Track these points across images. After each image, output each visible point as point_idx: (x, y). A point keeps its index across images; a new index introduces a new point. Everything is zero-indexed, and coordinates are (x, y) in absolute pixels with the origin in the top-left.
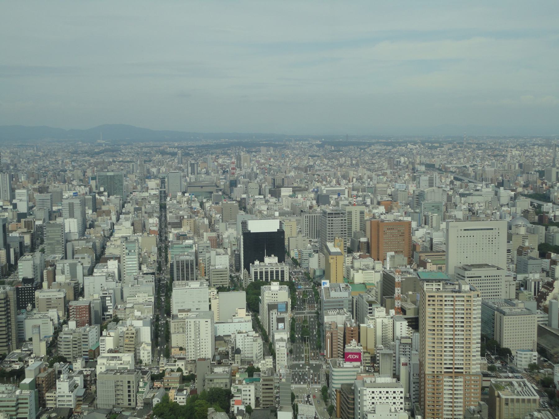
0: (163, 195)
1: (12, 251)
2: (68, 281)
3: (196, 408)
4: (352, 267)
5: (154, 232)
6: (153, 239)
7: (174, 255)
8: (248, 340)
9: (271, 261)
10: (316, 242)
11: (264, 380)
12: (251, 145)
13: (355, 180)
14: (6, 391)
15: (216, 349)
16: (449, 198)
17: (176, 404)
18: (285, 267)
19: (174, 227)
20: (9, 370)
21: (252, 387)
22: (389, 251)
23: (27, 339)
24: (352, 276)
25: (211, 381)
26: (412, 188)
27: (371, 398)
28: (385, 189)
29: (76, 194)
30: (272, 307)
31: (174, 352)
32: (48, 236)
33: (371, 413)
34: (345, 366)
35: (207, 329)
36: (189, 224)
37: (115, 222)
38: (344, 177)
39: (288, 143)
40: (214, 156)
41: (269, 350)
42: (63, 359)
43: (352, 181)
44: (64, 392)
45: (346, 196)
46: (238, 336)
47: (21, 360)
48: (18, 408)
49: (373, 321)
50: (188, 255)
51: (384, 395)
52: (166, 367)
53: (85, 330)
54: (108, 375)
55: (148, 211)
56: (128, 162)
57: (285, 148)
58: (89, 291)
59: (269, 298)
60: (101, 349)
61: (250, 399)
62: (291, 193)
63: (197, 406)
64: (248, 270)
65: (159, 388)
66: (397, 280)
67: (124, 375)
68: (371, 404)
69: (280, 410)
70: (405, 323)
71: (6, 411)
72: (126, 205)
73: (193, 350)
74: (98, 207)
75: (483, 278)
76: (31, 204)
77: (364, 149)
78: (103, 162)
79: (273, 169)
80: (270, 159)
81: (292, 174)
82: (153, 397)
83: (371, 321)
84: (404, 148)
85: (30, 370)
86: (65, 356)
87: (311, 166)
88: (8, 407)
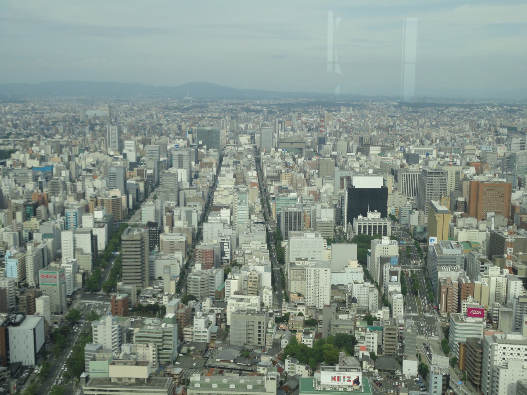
0: (257, 151)
1: (131, 196)
2: (186, 226)
3: (325, 351)
4: (455, 226)
8: (364, 291)
9: (374, 216)
10: (413, 200)
11: (387, 329)
12: (331, 104)
13: (438, 141)
14: (153, 324)
15: (332, 297)
17: (305, 346)
18: (388, 223)
19: (274, 181)
20: (145, 304)
21: (376, 335)
22: (489, 212)
23: (157, 278)
24: (455, 233)
25: (336, 326)
26: (501, 150)
27: (502, 354)
28: (474, 151)
30: (384, 260)
31: (293, 297)
32: (163, 184)
33: (503, 368)
34: (467, 321)
35: (326, 278)
36: (287, 177)
39: (365, 103)
41: (384, 301)
42: (193, 298)
43: (436, 142)
44: (200, 328)
45: (434, 155)
46: (355, 286)
47: (154, 296)
48: (164, 340)
49: (487, 279)
50: (295, 207)
51: (515, 352)
52: (288, 311)
53: (212, 272)
54: (240, 315)
55: (245, 165)
56: (216, 118)
57: (363, 108)
58: (207, 237)
59: (380, 252)
60: (226, 290)
61: (373, 346)
62: (380, 152)
63: (325, 349)
64: (352, 224)
65: (284, 330)
67: (255, 316)
68: (502, 359)
69: (405, 359)
70: (520, 283)
71: (155, 342)
72: (224, 158)
73: (312, 297)
74: (199, 159)
76: (138, 154)
77: (442, 111)
78: (194, 118)
79: (355, 128)
80: (351, 118)
81: (375, 133)
82: (281, 338)
83: (485, 279)
84: (482, 110)
85: (171, 306)
86: (195, 295)
87: (392, 127)
88: (155, 338)
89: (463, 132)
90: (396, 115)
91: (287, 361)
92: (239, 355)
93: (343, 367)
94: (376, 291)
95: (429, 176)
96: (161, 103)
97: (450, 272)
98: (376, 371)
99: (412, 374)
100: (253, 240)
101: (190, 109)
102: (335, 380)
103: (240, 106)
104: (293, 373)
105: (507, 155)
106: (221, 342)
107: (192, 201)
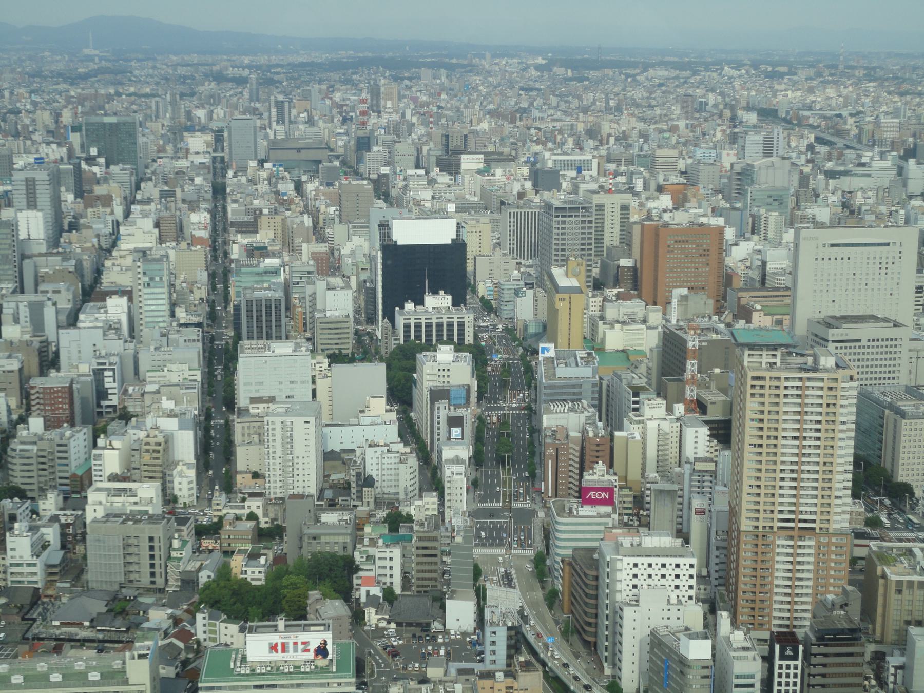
0: (218, 169)
2: (27, 337)
4: (602, 318)
5: (200, 241)
6: (200, 254)
7: (240, 288)
8: (389, 461)
9: (438, 303)
10: (531, 266)
11: (420, 539)
12: (401, 65)
13: (612, 140)
16: (804, 180)
18: (466, 316)
21: (397, 552)
22: (677, 287)
24: (600, 335)
25: (315, 538)
26: (728, 158)
28: (673, 160)
29: (39, 161)
30: (438, 395)
31: (243, 481)
33: (629, 605)
34: (581, 513)
36: (272, 224)
37: (121, 219)
38: (592, 133)
39: (476, 61)
40: (324, 87)
41: (432, 479)
43: (608, 143)
44: (21, 557)
45: (594, 172)
46: (370, 452)
49: (640, 425)
50: (269, 289)
51: (656, 571)
52: (224, 512)
53: (62, 436)
54: (109, 524)
55: (188, 199)
56: (146, 96)
57: (470, 71)
58: (69, 358)
60: (94, 473)
61: (391, 576)
62: (481, 166)
65: (211, 551)
66: (690, 345)
67: (141, 525)
69: (451, 598)
73: (278, 478)
74: (86, 188)
75: (864, 342)
77: (634, 76)
78: (96, 96)
79: (446, 116)
80: (439, 94)
82: (200, 569)
83: (636, 426)
84: (715, 74)
86: (23, 487)
87: (524, 111)
89: (666, 121)
90: (537, 85)
91: (199, 616)
92: (104, 610)
93: (317, 622)
94: (413, 462)
95: (558, 216)
96: (28, 62)
97: (566, 415)
98: (393, 625)
99: (463, 629)
100: (172, 361)
101: (91, 77)
102: (276, 651)
103: (202, 69)
104: (214, 640)
105: (738, 168)
106: (68, 585)
107: (52, 282)
